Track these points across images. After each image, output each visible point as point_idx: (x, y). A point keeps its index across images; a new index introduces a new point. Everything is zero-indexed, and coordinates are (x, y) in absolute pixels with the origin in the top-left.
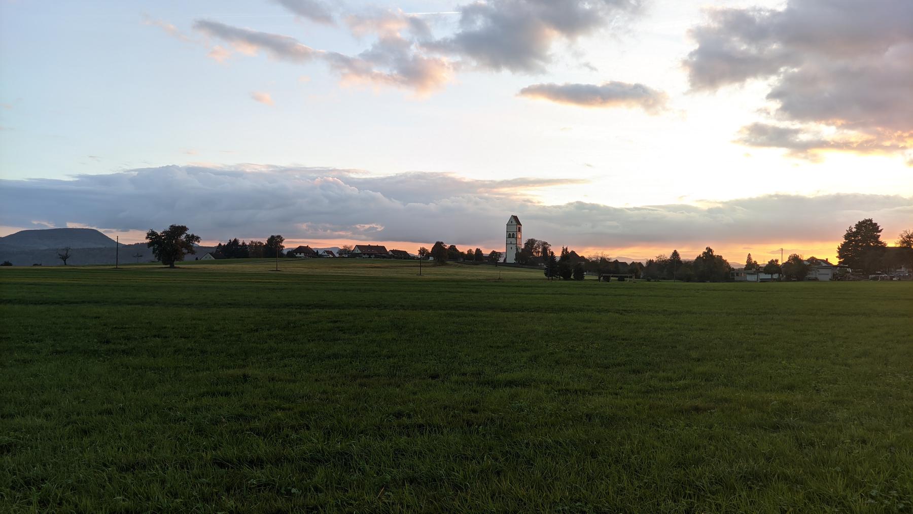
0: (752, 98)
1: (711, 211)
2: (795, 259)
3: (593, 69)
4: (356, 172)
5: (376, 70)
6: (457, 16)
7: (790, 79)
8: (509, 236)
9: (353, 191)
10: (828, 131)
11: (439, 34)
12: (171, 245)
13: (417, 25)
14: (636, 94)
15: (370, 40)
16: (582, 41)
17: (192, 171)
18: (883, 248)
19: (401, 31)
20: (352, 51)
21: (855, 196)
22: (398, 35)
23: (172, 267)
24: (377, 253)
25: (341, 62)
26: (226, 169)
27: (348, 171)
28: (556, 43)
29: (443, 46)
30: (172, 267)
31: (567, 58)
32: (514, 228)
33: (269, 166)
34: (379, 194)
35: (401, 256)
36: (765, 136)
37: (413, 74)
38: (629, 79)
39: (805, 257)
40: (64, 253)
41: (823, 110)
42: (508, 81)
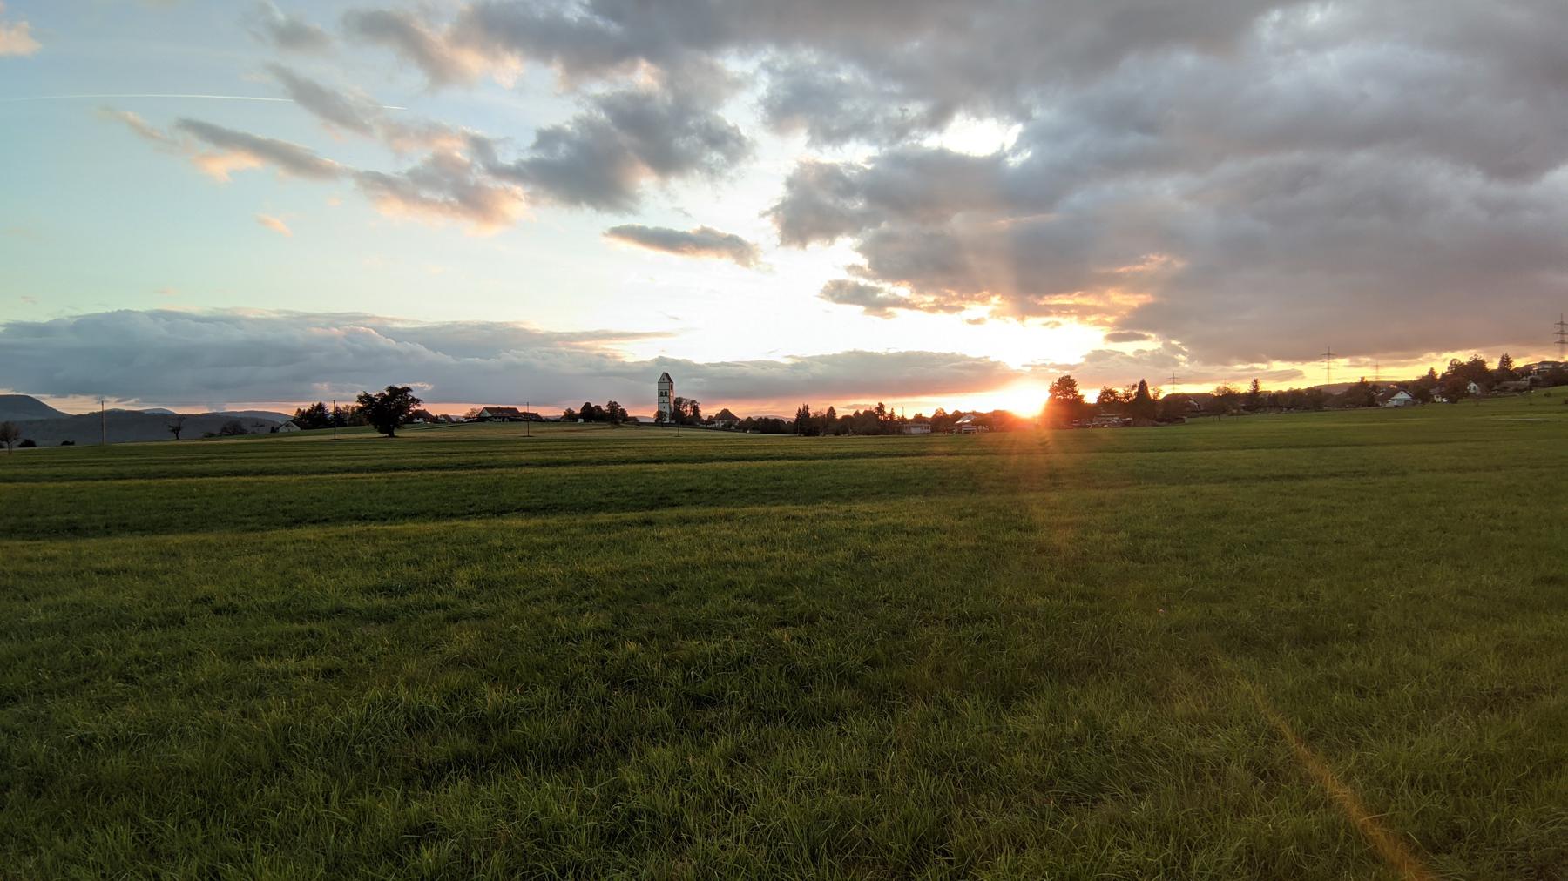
0: (841, 255)
1: (795, 366)
2: (366, 399)
3: (687, 215)
4: (402, 321)
5: (426, 194)
6: (532, 139)
7: (1041, 298)
8: (661, 395)
9: (391, 343)
10: (903, 290)
11: (509, 158)
12: (389, 411)
13: (480, 146)
14: (734, 247)
15: (418, 156)
16: (675, 183)
17: (155, 315)
18: (1089, 405)
19: (461, 153)
20: (387, 167)
21: (920, 353)
22: (458, 155)
23: (392, 435)
24: (511, 416)
25: (379, 184)
26: (818, 370)
27: (393, 320)
28: (646, 182)
29: (516, 174)
30: (392, 435)
31: (663, 200)
32: (666, 386)
33: (279, 312)
34: (422, 348)
35: (535, 418)
36: (842, 293)
37: (473, 202)
38: (723, 229)
39: (949, 412)
40: (175, 424)
41: (895, 275)
42: (587, 224)
